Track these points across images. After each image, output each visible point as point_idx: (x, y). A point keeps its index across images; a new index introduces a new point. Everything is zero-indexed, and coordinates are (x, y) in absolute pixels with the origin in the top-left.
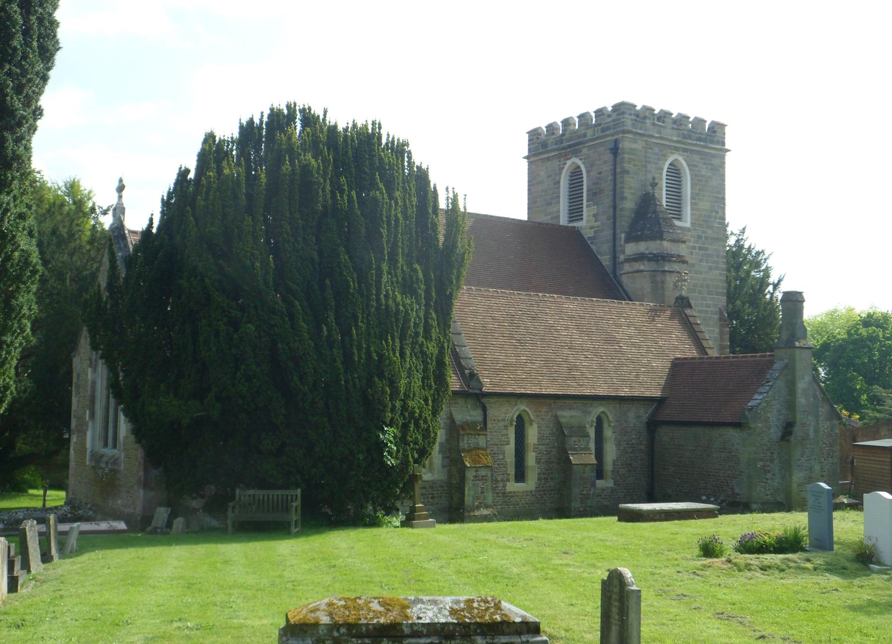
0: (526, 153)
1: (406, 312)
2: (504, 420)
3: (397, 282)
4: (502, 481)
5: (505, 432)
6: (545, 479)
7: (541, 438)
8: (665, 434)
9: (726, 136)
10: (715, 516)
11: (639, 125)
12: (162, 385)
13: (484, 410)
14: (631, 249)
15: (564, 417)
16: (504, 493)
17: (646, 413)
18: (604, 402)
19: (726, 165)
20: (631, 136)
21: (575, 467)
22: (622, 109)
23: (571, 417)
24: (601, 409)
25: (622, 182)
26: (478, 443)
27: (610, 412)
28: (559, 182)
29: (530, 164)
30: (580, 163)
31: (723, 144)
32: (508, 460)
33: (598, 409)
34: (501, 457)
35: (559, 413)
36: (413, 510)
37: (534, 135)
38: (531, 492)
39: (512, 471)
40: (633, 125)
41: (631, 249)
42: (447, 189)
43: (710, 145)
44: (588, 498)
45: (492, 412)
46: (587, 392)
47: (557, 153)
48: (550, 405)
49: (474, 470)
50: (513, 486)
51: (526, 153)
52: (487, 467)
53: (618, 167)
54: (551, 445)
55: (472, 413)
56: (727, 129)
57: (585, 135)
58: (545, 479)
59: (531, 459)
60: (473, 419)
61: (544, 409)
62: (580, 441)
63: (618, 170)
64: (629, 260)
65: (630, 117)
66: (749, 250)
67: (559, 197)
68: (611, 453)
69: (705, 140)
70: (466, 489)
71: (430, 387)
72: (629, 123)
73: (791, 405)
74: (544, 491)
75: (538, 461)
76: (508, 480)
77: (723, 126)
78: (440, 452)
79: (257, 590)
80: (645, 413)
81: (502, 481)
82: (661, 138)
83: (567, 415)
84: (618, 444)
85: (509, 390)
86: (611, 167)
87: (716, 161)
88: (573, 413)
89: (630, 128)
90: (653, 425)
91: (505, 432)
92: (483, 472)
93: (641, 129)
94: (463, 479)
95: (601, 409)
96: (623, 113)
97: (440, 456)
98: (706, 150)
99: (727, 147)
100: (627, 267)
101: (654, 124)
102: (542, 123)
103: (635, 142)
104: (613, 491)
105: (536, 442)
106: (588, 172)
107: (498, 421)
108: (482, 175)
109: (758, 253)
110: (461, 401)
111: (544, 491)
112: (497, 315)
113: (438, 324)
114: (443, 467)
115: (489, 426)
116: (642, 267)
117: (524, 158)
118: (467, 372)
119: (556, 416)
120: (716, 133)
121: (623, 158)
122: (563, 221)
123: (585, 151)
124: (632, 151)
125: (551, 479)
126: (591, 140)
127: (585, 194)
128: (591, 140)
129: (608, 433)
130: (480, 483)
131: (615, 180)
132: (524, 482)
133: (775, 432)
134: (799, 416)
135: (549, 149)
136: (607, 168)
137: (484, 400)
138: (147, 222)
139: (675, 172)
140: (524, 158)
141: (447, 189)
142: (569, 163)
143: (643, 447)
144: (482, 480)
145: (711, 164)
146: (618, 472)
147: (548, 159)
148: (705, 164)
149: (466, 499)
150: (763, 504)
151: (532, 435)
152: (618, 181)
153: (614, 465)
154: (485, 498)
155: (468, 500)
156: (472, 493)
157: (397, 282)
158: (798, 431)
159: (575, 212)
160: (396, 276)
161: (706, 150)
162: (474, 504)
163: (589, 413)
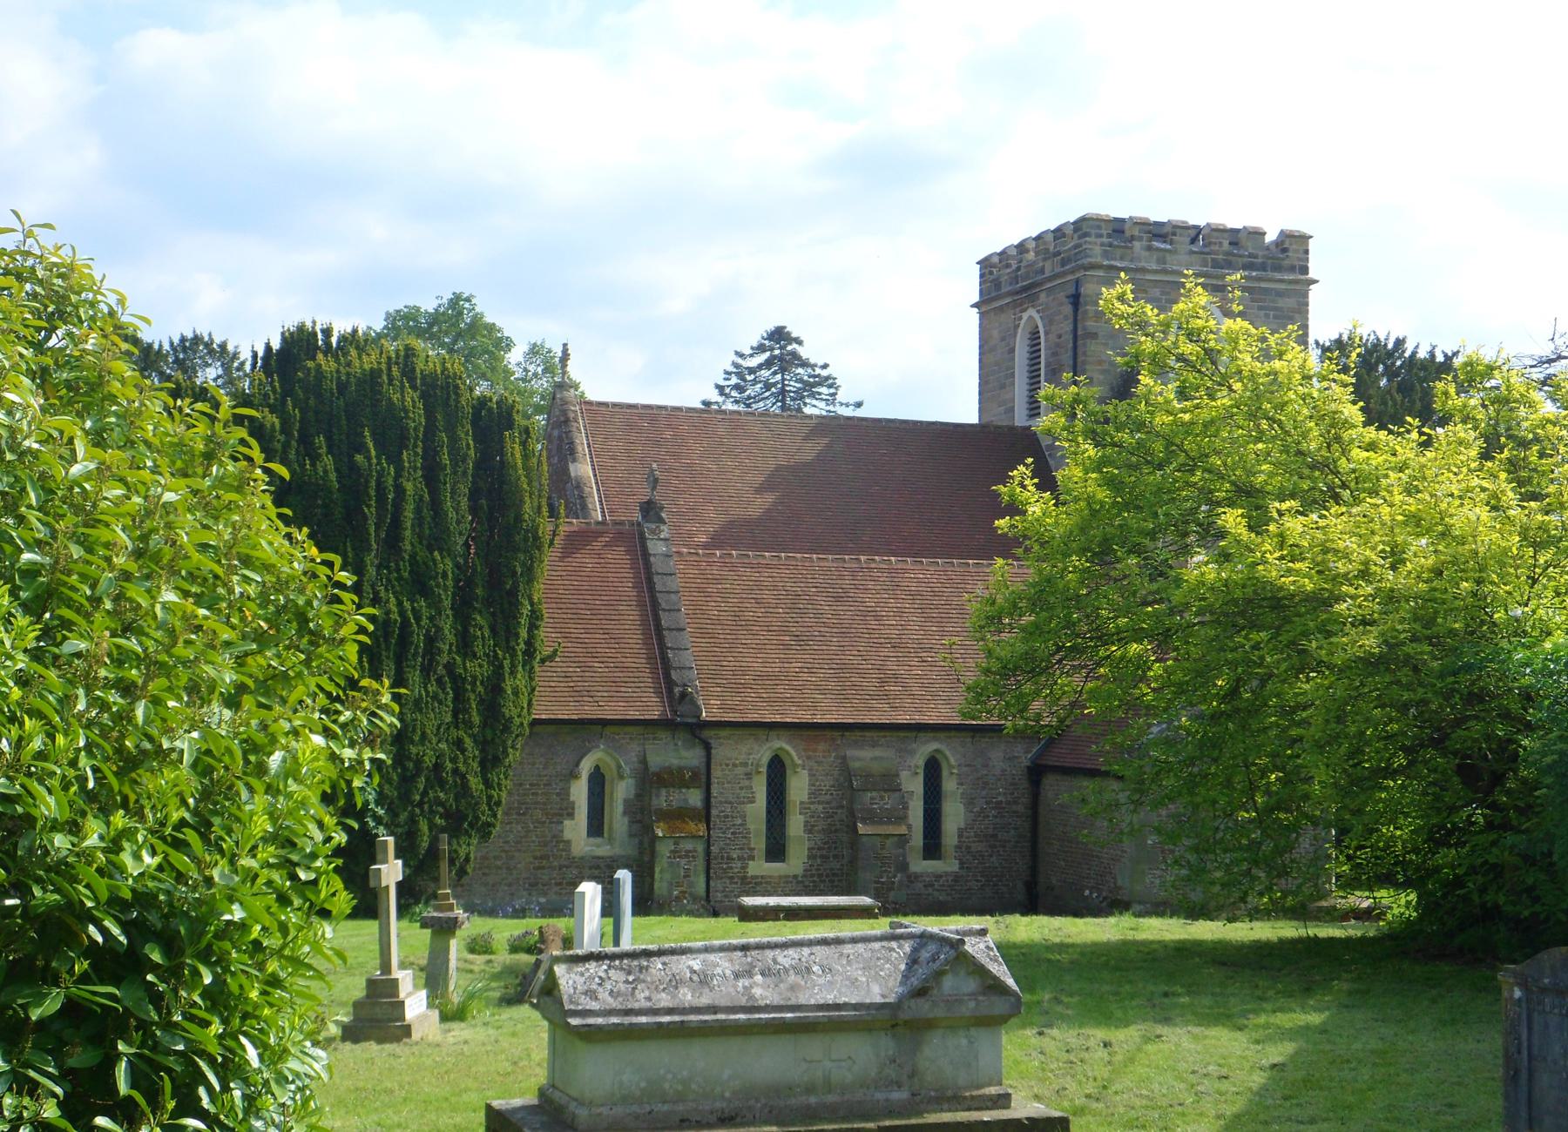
0: (976, 298)
1: (405, 623)
2: (745, 764)
3: (400, 579)
4: (739, 858)
5: (747, 783)
6: (822, 857)
7: (814, 794)
8: (1058, 792)
9: (1311, 256)
10: (875, 917)
11: (1119, 252)
13: (708, 748)
15: (859, 759)
16: (744, 878)
17: (1027, 752)
18: (942, 735)
19: (1310, 308)
20: (1101, 273)
21: (864, 839)
23: (876, 758)
24: (934, 746)
25: (1084, 353)
26: (686, 800)
27: (952, 755)
28: (1012, 350)
29: (983, 316)
31: (1305, 270)
32: (752, 827)
33: (925, 749)
34: (739, 821)
35: (850, 753)
38: (795, 877)
39: (759, 844)
40: (1106, 255)
43: (1278, 276)
44: (890, 889)
45: (719, 753)
46: (903, 718)
47: (1008, 300)
48: (833, 740)
49: (671, 842)
50: (919, 866)
52: (694, 837)
53: (1080, 326)
54: (834, 804)
55: (684, 753)
56: (1312, 244)
57: (1042, 271)
58: (822, 857)
59: (795, 825)
60: (683, 763)
61: (821, 747)
62: (882, 798)
63: (1080, 332)
65: (1099, 240)
67: (1013, 375)
68: (954, 816)
69: (1263, 267)
70: (657, 870)
71: (469, 725)
72: (1098, 250)
74: (820, 876)
75: (809, 828)
76: (752, 858)
77: (1303, 239)
78: (625, 813)
80: (1024, 756)
81: (739, 858)
82: (1165, 271)
83: (865, 757)
84: (969, 802)
85: (753, 717)
86: (1071, 327)
87: (1287, 303)
88: (877, 752)
89: (1099, 260)
90: (1036, 773)
91: (747, 783)
92: (688, 845)
93: (1122, 259)
94: (653, 853)
95: (934, 746)
96: (1086, 235)
97: (626, 820)
98: (1263, 285)
99: (1312, 274)
101: (1149, 248)
104: (957, 878)
105: (805, 798)
106: (1046, 333)
107: (735, 765)
110: (664, 735)
111: (820, 876)
112: (766, 595)
113: (493, 630)
114: (631, 835)
117: (975, 305)
118: (677, 690)
119: (844, 758)
121: (1086, 312)
122: (1020, 419)
123: (1043, 295)
125: (835, 857)
126: (1050, 279)
127: (1042, 372)
128: (1050, 279)
129: (949, 785)
130: (683, 861)
131: (1075, 348)
132: (939, 858)
136: (1067, 327)
137: (706, 734)
138: (794, 335)
140: (975, 305)
142: (1025, 316)
143: (1020, 808)
144: (687, 856)
145: (1276, 309)
146: (968, 847)
147: (1001, 309)
148: (1260, 308)
149: (656, 885)
150: (1157, 905)
151: (798, 788)
152: (1080, 351)
153: (960, 836)
154: (691, 885)
156: (667, 876)
157: (400, 579)
160: (398, 570)
161: (1263, 285)
162: (670, 893)
163: (912, 753)
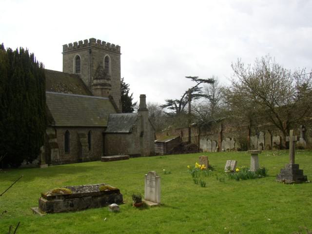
0: (62, 52)
12: (305, 119)
13: (56, 131)
14: (95, 82)
22: (93, 40)
30: (79, 55)
36: (40, 161)
37: (65, 47)
41: (95, 82)
42: (232, 66)
51: (62, 51)
64: (94, 85)
66: (125, 83)
73: (142, 126)
79: (128, 186)
90: (104, 134)
100: (94, 87)
102: (68, 43)
103: (96, 49)
108: (51, 60)
109: (127, 85)
115: (57, 135)
116: (99, 87)
120: (118, 47)
124: (95, 53)
133: (139, 134)
134: (145, 130)
135: (69, 50)
139: (107, 58)
141: (232, 66)
155: (52, 158)
158: (145, 134)
159: (78, 70)
